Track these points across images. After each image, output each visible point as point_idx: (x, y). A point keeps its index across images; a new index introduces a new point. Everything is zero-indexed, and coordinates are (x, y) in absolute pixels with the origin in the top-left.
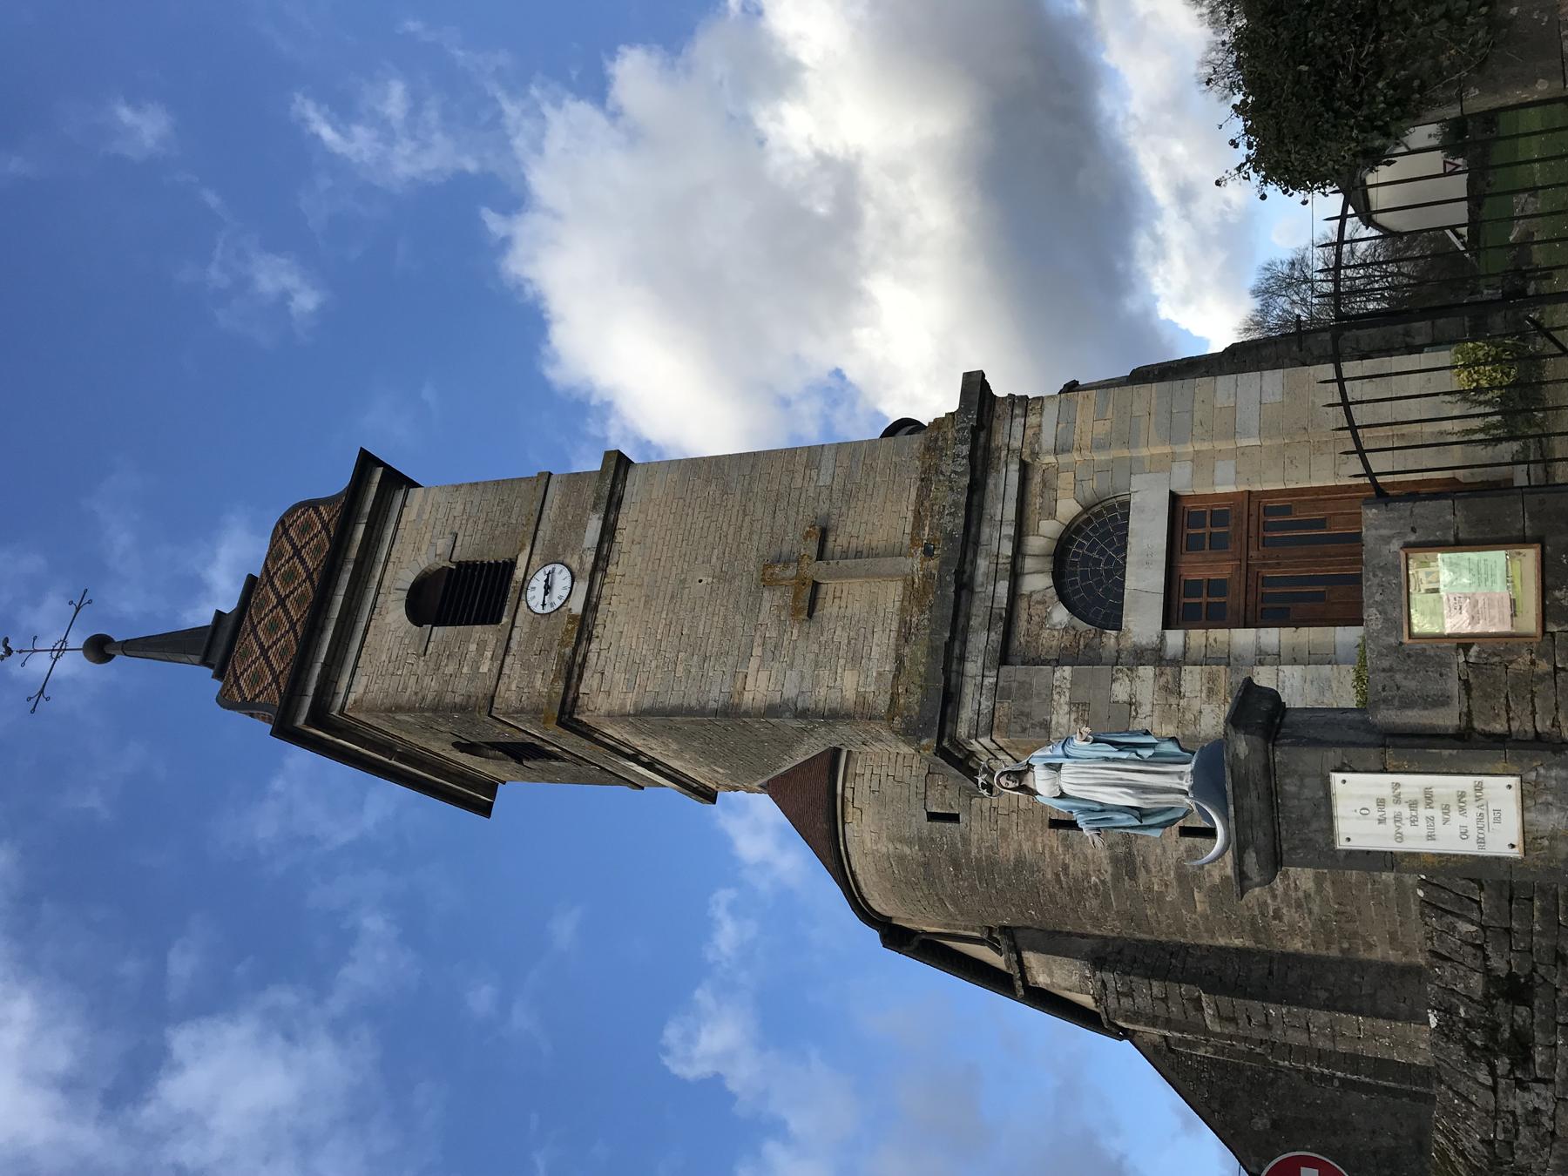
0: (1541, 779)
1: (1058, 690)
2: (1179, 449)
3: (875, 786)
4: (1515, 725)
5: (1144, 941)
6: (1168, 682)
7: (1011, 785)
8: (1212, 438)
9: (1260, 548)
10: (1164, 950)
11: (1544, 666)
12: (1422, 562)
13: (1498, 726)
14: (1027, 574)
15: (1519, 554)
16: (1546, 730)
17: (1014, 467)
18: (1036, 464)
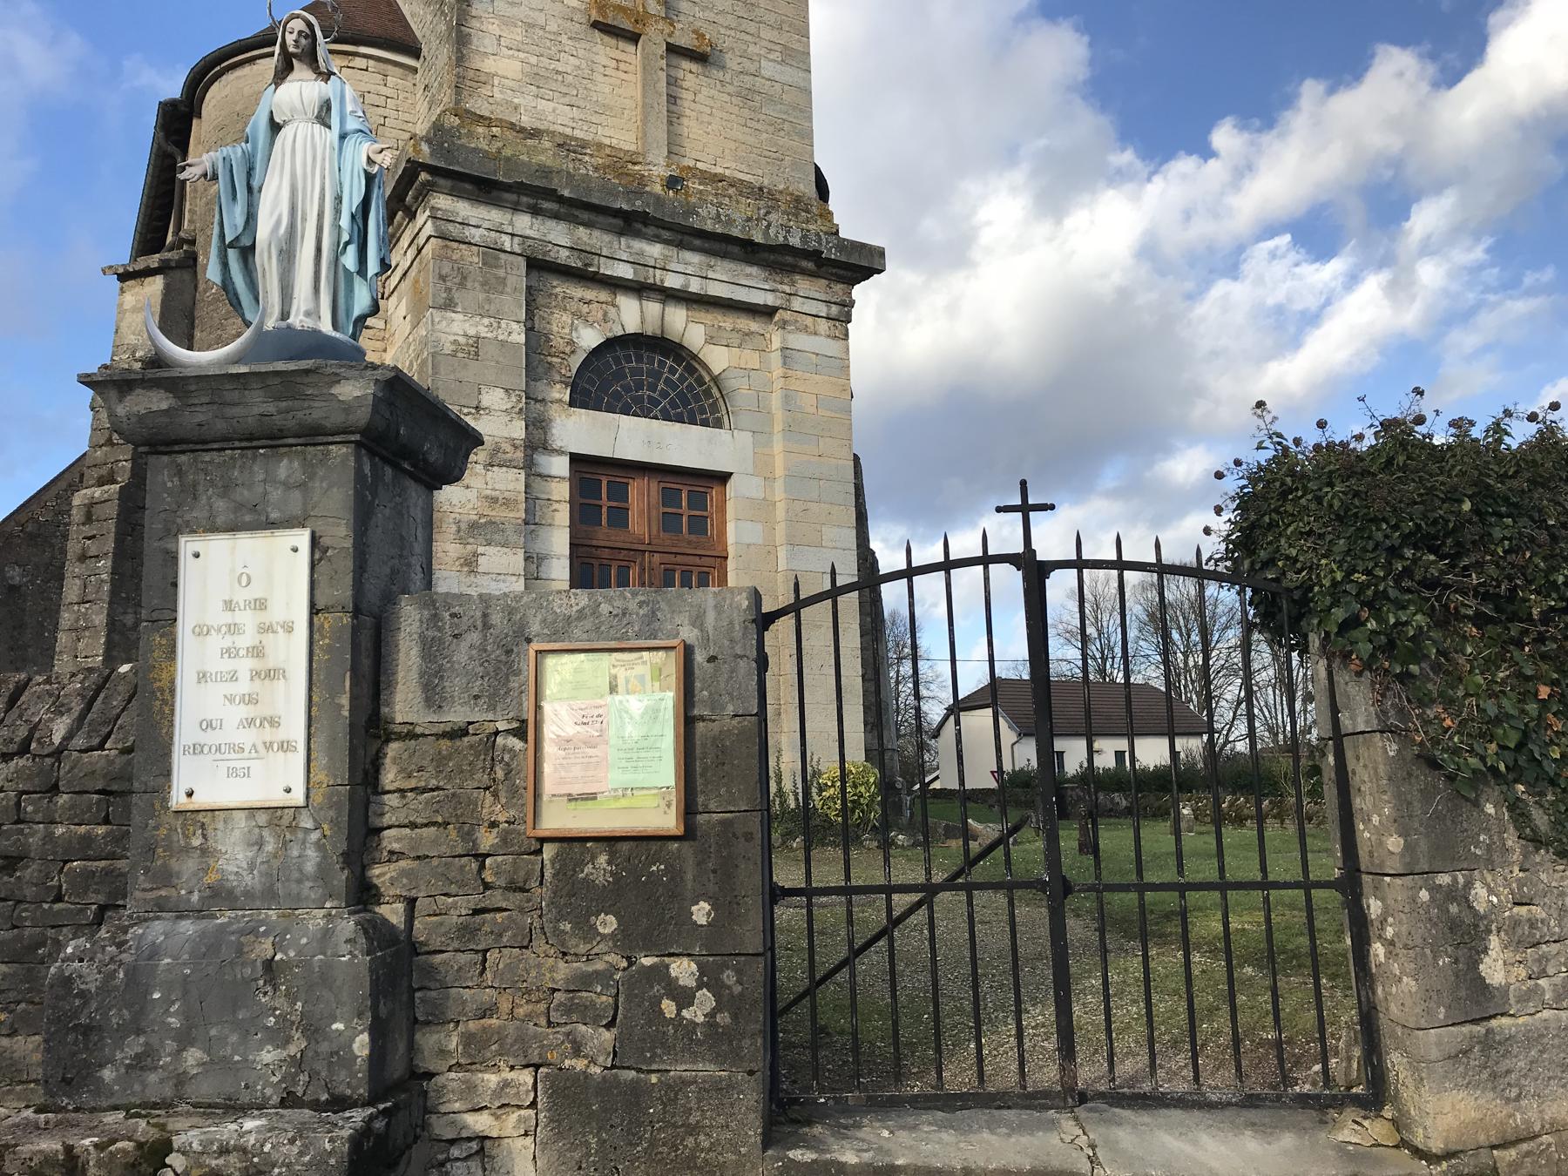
0: (300, 835)
2: (779, 485)
6: (505, 453)
8: (789, 520)
12: (660, 670)
15: (669, 806)
16: (385, 843)
17: (770, 299)
18: (771, 327)
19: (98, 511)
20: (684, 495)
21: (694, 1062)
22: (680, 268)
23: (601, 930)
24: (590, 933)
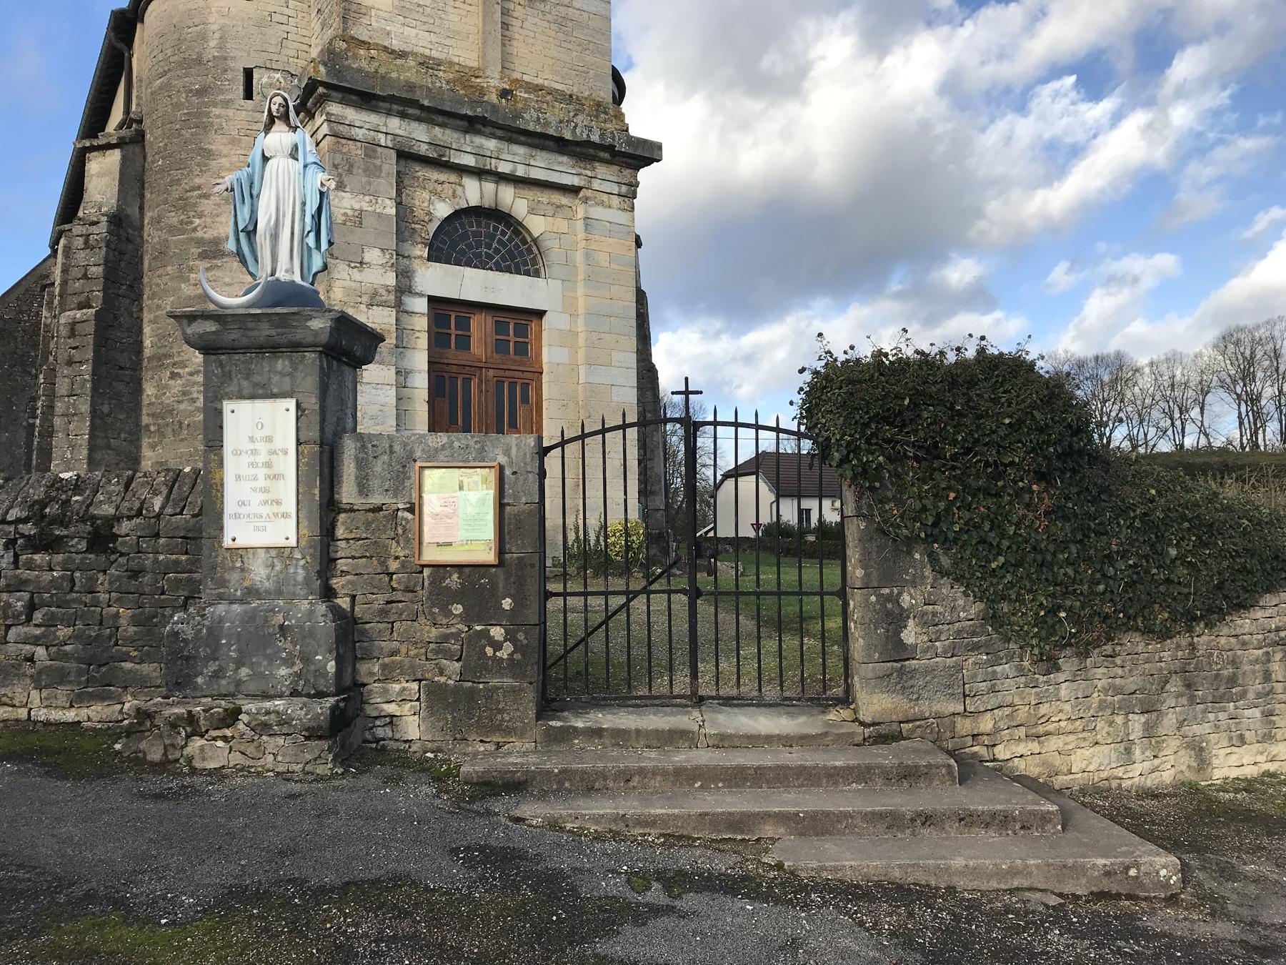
0: (294, 562)
3: (276, 18)
4: (342, 544)
5: (142, 264)
7: (274, 108)
10: (135, 279)
11: (394, 566)
13: (341, 532)
19: (78, 327)
20: (511, 327)
21: (502, 677)
22: (509, 158)
24: (448, 614)
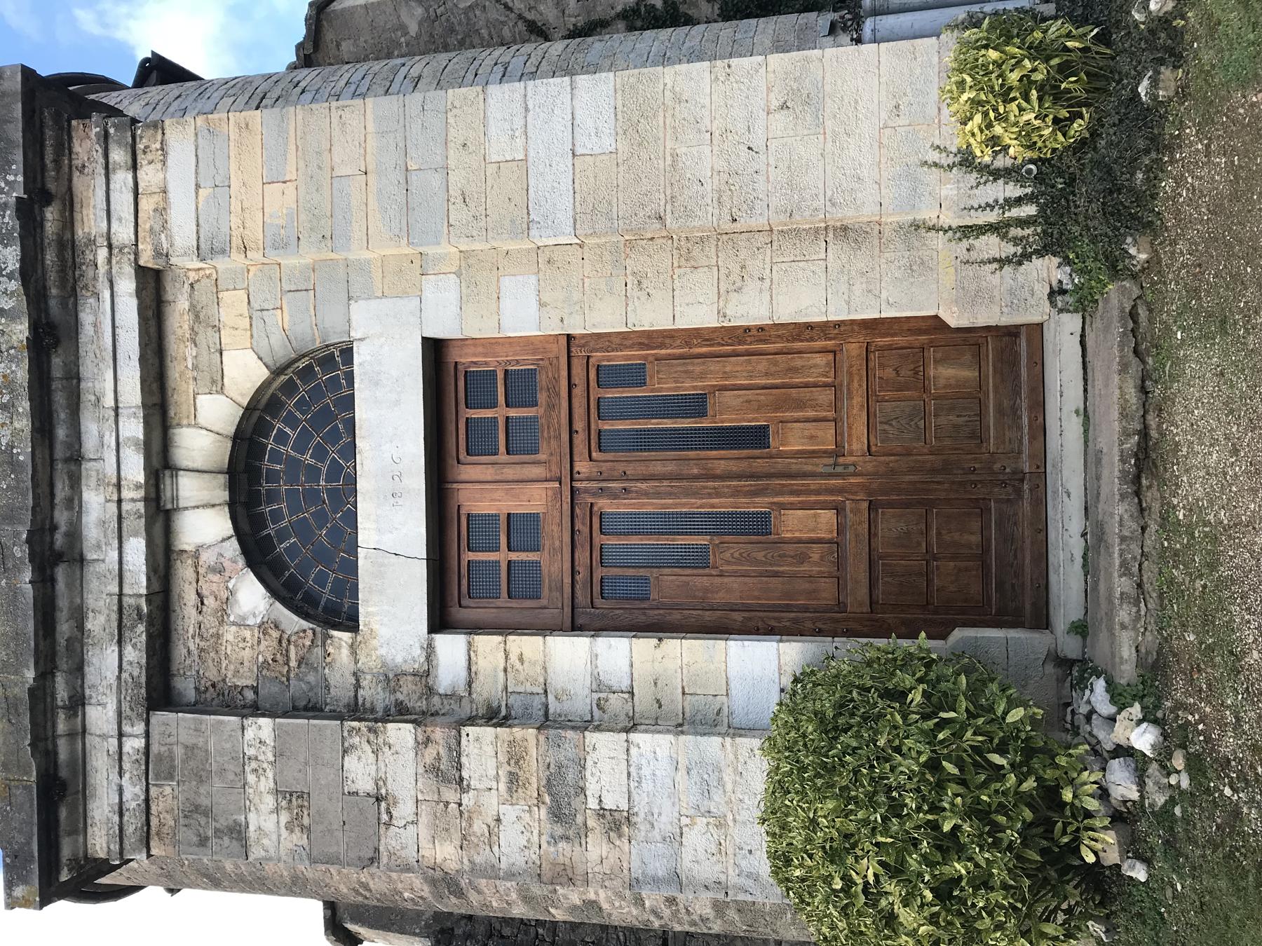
1: (254, 765)
6: (438, 758)
9: (594, 455)
14: (186, 508)
17: (127, 286)
23: (1035, 171)
